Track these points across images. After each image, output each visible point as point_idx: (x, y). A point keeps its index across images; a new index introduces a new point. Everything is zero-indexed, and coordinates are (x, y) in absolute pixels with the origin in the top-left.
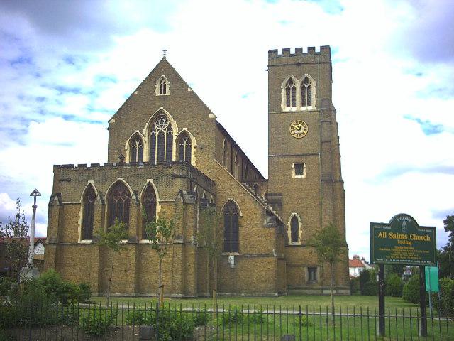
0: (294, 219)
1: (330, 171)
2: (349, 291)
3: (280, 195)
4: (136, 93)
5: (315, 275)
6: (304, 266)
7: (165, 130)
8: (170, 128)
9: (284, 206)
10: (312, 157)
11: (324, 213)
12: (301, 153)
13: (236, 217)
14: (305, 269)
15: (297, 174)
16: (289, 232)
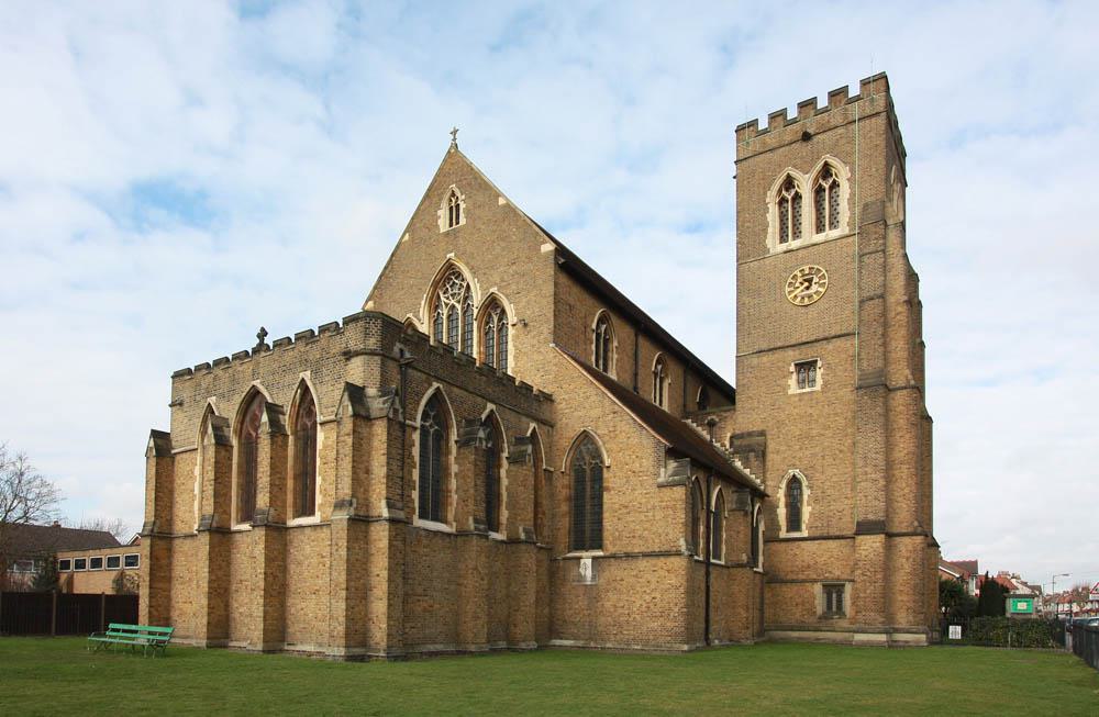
0: (794, 482)
1: (880, 364)
2: (923, 637)
3: (762, 433)
4: (407, 237)
5: (840, 601)
6: (815, 581)
7: (459, 302)
9: (770, 456)
10: (838, 342)
11: (861, 463)
12: (813, 338)
13: (598, 471)
14: (818, 588)
15: (801, 383)
16: (782, 512)
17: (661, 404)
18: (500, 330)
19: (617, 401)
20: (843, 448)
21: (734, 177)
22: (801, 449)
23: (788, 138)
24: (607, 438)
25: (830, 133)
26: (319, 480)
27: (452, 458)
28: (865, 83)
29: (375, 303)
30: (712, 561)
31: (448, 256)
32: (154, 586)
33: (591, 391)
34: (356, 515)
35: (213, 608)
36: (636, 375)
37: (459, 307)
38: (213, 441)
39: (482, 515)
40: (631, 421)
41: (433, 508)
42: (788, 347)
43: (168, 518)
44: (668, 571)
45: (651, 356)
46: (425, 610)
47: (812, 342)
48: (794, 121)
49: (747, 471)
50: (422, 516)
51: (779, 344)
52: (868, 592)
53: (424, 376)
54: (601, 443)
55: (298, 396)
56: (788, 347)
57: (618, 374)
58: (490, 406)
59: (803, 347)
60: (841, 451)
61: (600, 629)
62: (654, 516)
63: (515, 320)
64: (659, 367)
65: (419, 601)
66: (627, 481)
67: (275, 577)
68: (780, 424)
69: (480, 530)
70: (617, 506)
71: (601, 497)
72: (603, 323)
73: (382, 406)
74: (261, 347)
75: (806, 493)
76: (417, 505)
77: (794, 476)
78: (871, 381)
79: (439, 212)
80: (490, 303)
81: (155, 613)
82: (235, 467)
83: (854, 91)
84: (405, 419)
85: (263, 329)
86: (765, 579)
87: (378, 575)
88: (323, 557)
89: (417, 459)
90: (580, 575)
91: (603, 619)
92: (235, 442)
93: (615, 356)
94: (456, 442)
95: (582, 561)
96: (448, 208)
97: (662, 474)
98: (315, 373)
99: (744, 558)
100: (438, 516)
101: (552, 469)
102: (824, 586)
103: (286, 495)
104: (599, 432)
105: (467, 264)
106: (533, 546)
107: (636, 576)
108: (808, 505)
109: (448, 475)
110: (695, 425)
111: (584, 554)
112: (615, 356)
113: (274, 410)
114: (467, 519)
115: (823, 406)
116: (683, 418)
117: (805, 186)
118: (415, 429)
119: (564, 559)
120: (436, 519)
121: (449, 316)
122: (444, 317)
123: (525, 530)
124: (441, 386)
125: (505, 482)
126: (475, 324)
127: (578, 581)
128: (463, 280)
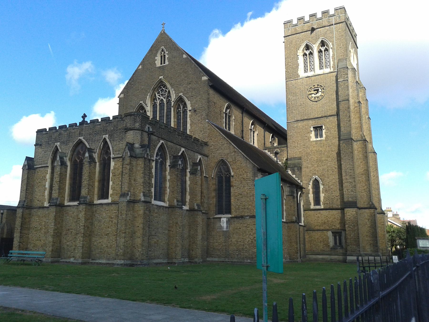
3: (300, 158)
4: (140, 67)
6: (328, 230)
7: (165, 98)
8: (169, 96)
9: (303, 170)
12: (320, 116)
14: (330, 234)
15: (316, 137)
17: (254, 144)
18: (183, 112)
19: (236, 147)
21: (284, 42)
22: (318, 166)
23: (306, 29)
24: (232, 163)
26: (111, 183)
27: (167, 173)
28: (336, 10)
29: (124, 95)
31: (160, 77)
32: (22, 232)
33: (225, 142)
34: (130, 200)
36: (242, 131)
37: (165, 100)
38: (60, 164)
39: (180, 198)
40: (242, 156)
41: (159, 196)
42: (309, 119)
43: (31, 198)
46: (155, 243)
47: (320, 118)
48: (308, 22)
49: (294, 176)
50: (155, 200)
51: (306, 118)
52: (352, 235)
53: (157, 138)
54: (229, 165)
55: (102, 145)
56: (309, 119)
57: (235, 131)
58: (183, 149)
59: (316, 119)
61: (230, 252)
63: (191, 108)
64: (253, 126)
65: (153, 238)
66: (241, 183)
67: (88, 227)
69: (179, 205)
70: (237, 194)
71: (230, 189)
72: (228, 109)
73: (142, 152)
74: (83, 123)
75: (321, 187)
76: (153, 194)
77: (315, 179)
78: (346, 137)
79: (156, 58)
80: (179, 100)
81: (21, 246)
82: (68, 175)
83: (332, 12)
84: (151, 157)
85: (84, 114)
86: (305, 229)
87: (138, 226)
88: (112, 218)
89: (154, 174)
91: (232, 247)
92: (69, 164)
94: (169, 166)
95: (222, 219)
96: (160, 56)
98: (111, 137)
99: (294, 218)
100: (161, 199)
101: (208, 176)
102: (332, 232)
103: (94, 189)
104: (228, 160)
105: (169, 82)
106: (200, 213)
107: (246, 227)
109: (165, 180)
110: (269, 153)
111: (223, 216)
112: (233, 123)
113: (91, 151)
114: (174, 201)
117: (315, 48)
118: (153, 161)
119: (214, 218)
120: (160, 200)
121: (160, 104)
122: (158, 104)
123: (197, 205)
124: (164, 142)
125: (188, 183)
126: (172, 109)
128: (167, 88)
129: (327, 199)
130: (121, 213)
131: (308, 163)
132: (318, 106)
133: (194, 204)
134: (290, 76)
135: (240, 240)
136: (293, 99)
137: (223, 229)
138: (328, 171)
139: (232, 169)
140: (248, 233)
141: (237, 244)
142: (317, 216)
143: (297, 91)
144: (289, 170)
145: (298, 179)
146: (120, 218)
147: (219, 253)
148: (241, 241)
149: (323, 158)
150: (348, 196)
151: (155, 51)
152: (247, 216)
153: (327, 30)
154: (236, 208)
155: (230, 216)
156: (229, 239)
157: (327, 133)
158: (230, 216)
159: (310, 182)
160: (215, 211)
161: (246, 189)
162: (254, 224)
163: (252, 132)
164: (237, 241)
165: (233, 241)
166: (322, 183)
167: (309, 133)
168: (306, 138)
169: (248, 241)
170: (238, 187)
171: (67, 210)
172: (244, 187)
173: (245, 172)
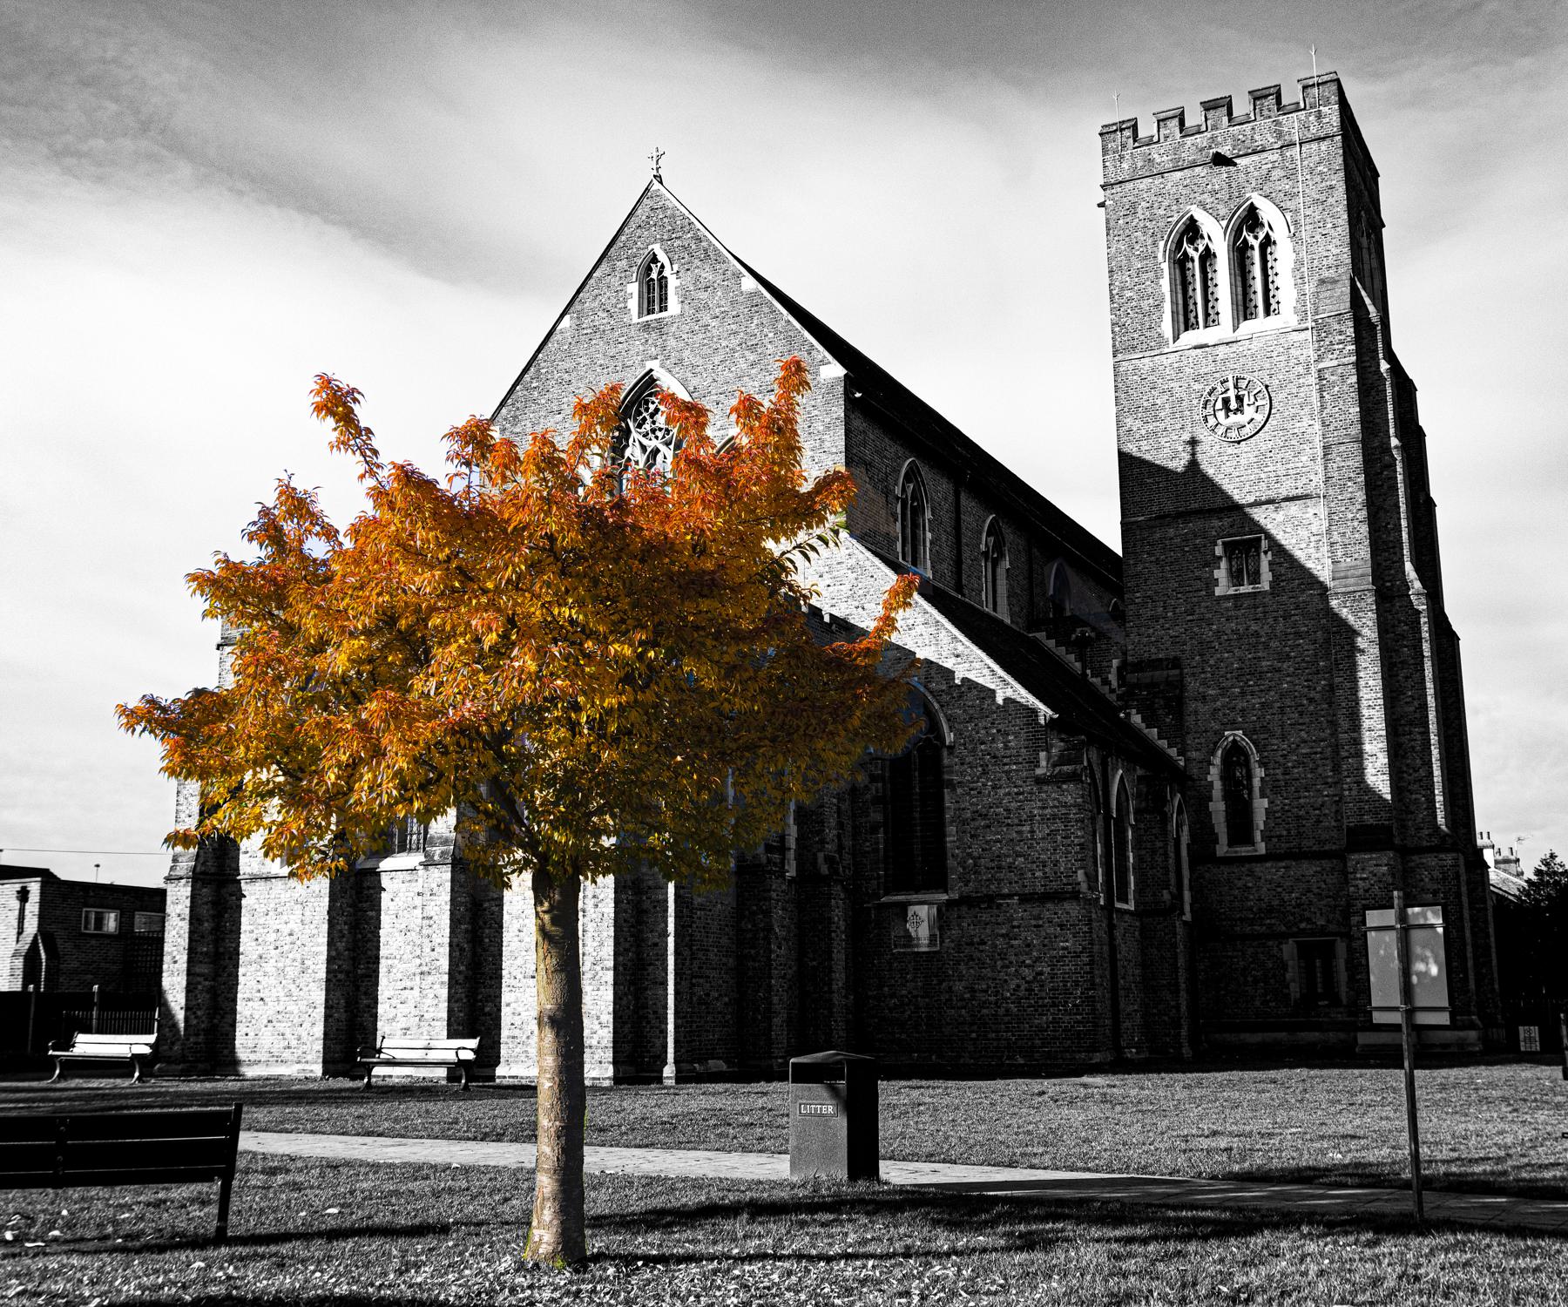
3: (1176, 663)
6: (1283, 937)
7: (667, 444)
14: (1289, 949)
15: (1236, 577)
17: (995, 610)
20: (1312, 694)
21: (1101, 205)
22: (1243, 693)
23: (1188, 156)
24: (945, 698)
25: (1255, 157)
30: (1118, 905)
35: (332, 1007)
36: (958, 562)
40: (986, 671)
44: (1061, 926)
45: (980, 522)
54: (937, 706)
60: (1311, 700)
62: (1032, 832)
66: (985, 772)
68: (1204, 647)
77: (1234, 740)
90: (908, 936)
93: (929, 535)
95: (912, 909)
97: (1043, 763)
108: (1263, 796)
111: (914, 897)
112: (929, 535)
115: (1276, 619)
116: (1030, 630)
117: (1216, 235)
127: (904, 946)
129: (1280, 821)
130: (594, 897)
131: (1204, 683)
132: (1243, 462)
133: (815, 854)
134: (1131, 342)
135: (984, 987)
136: (1143, 432)
137: (918, 946)
138: (1283, 713)
139: (949, 720)
140: (1013, 958)
141: (973, 998)
142: (1240, 884)
143: (1158, 402)
144: (1134, 711)
145: (1170, 746)
146: (594, 916)
147: (904, 1036)
148: (989, 987)
149: (1264, 664)
150: (1360, 809)
151: (624, 262)
152: (1010, 896)
153: (1270, 166)
154: (964, 868)
155: (945, 897)
156: (940, 983)
157: (1280, 564)
158: (945, 897)
159: (1213, 753)
160: (882, 880)
161: (1006, 794)
162: (1035, 926)
163: (989, 564)
164: (973, 991)
165: (955, 988)
166: (1261, 757)
167: (1207, 564)
168: (1199, 584)
169: (1013, 986)
170: (972, 789)
171: (369, 888)
172: (994, 787)
173: (999, 731)
